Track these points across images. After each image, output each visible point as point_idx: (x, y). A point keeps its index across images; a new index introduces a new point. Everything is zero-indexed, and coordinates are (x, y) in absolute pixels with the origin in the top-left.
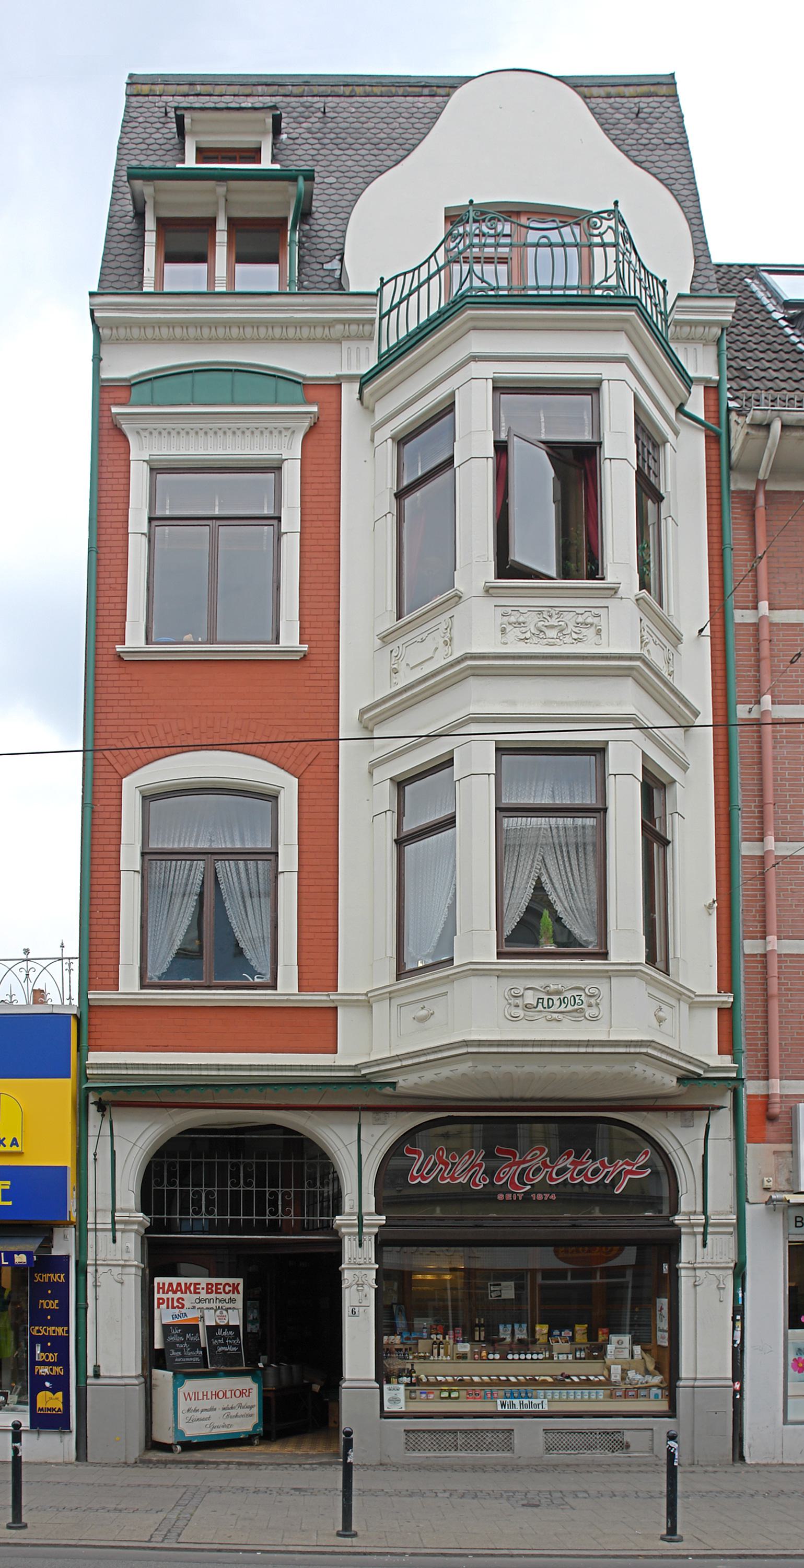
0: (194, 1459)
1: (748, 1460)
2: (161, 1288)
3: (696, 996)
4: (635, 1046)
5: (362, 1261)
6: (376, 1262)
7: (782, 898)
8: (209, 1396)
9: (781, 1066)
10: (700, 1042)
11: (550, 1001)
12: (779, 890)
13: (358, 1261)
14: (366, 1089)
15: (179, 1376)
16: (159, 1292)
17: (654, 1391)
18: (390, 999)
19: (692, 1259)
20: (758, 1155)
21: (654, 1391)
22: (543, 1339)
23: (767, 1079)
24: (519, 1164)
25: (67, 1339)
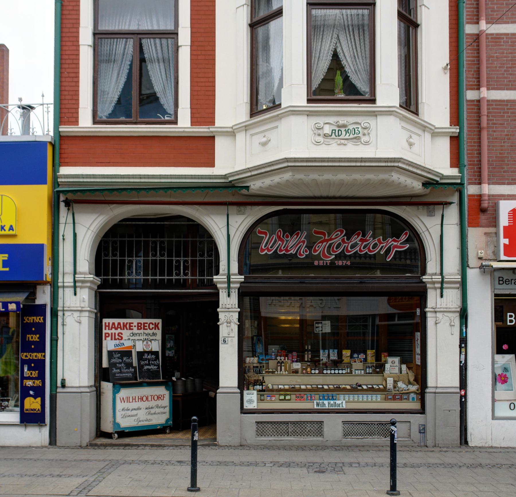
0: (124, 443)
1: (470, 444)
2: (108, 326)
3: (436, 128)
4: (391, 162)
5: (230, 306)
6: (239, 307)
7: (490, 62)
8: (137, 400)
9: (489, 175)
10: (436, 158)
11: (340, 132)
12: (488, 57)
13: (228, 306)
14: (230, 191)
15: (117, 386)
16: (105, 329)
17: (412, 395)
18: (246, 130)
19: (434, 306)
20: (475, 235)
21: (412, 395)
22: (346, 360)
23: (480, 184)
24: (327, 241)
25: (44, 361)
